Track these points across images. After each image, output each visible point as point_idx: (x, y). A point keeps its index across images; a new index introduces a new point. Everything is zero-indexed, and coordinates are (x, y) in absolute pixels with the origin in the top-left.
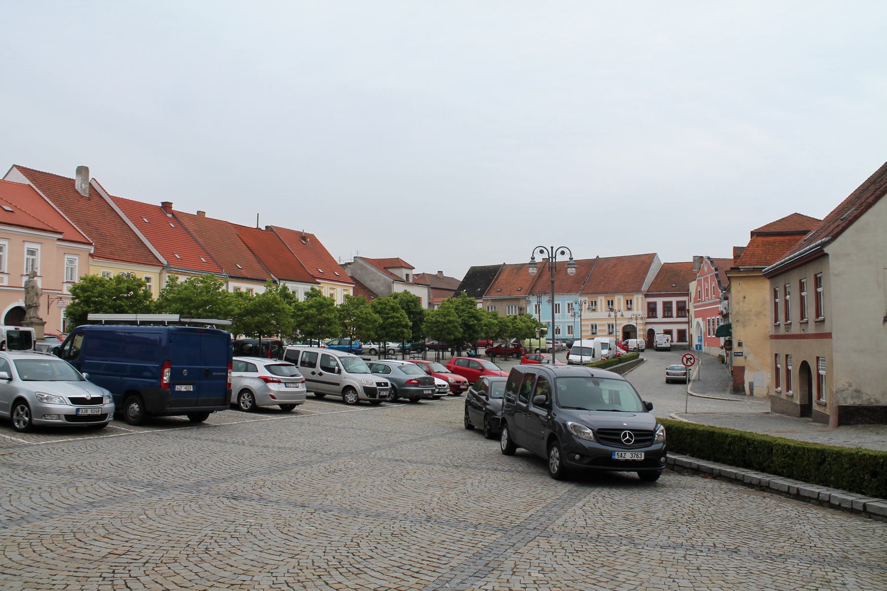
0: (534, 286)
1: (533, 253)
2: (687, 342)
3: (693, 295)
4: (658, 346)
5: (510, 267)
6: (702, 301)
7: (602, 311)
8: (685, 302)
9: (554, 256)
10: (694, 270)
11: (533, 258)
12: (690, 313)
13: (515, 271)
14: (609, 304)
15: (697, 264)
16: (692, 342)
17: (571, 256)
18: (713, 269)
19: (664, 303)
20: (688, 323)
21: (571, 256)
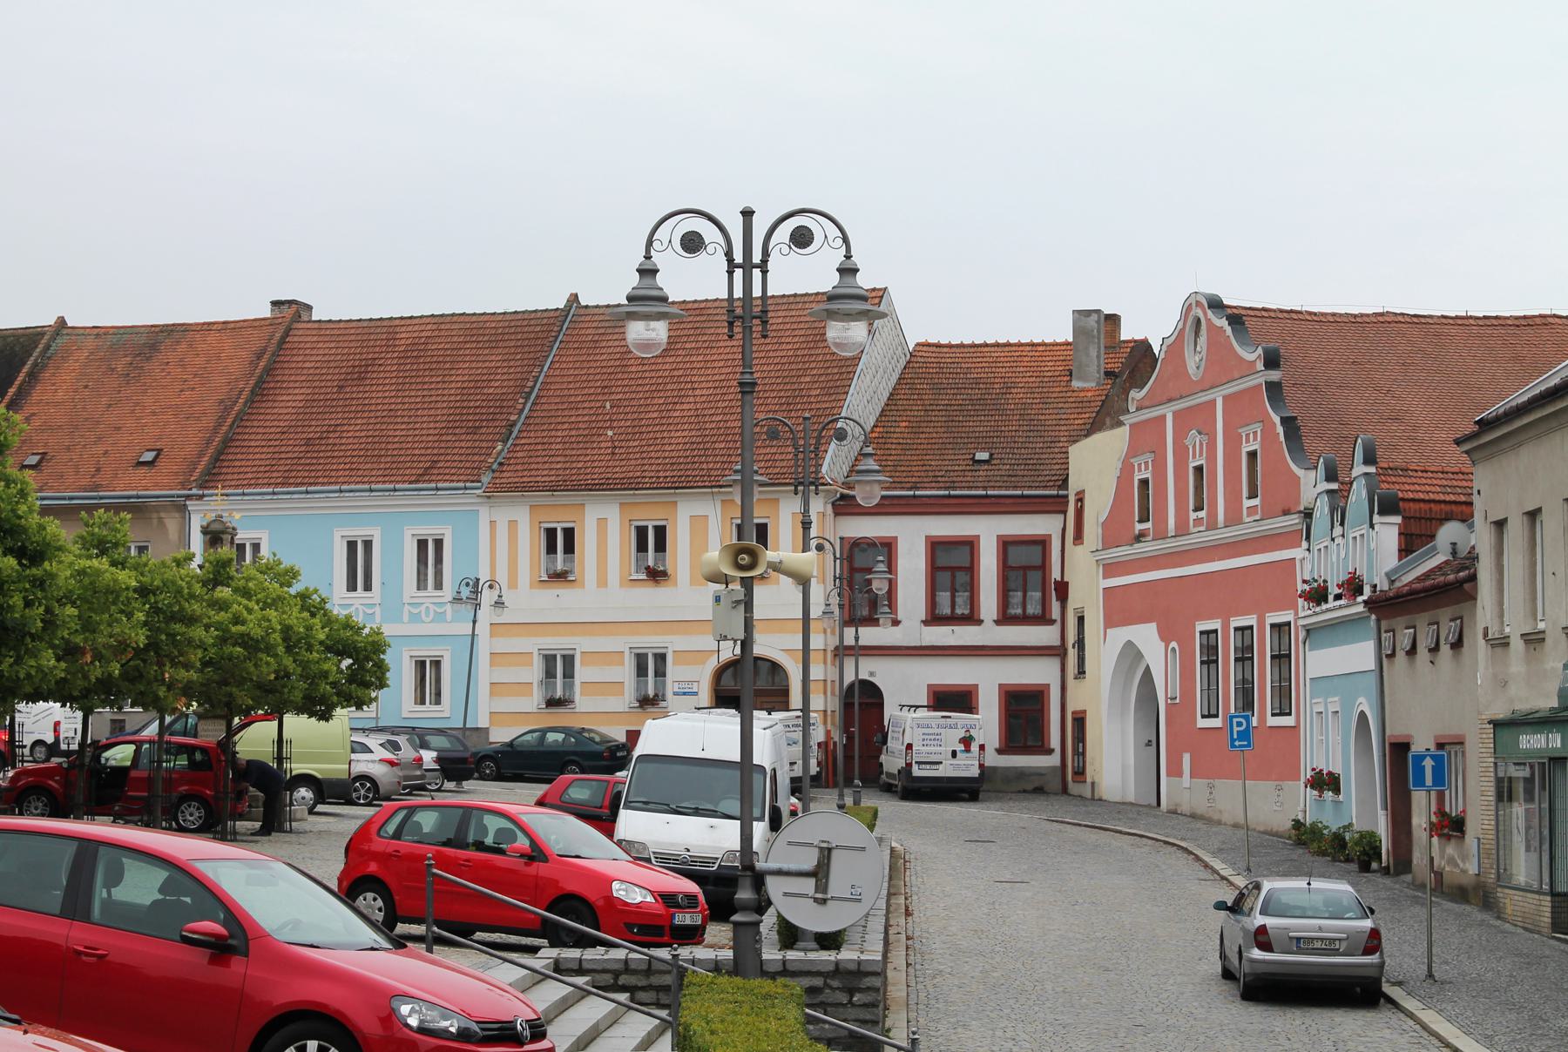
0: (227, 443)
1: (650, 243)
2: (1050, 752)
3: (1098, 509)
4: (917, 772)
5: (90, 343)
6: (1161, 535)
7: (602, 582)
8: (1042, 543)
9: (757, 258)
10: (1076, 384)
11: (648, 272)
12: (1073, 603)
13: (121, 365)
14: (642, 547)
15: (1093, 353)
16: (1080, 754)
17: (848, 257)
18: (1253, 356)
19: (936, 546)
20: (1059, 652)
21: (848, 257)
